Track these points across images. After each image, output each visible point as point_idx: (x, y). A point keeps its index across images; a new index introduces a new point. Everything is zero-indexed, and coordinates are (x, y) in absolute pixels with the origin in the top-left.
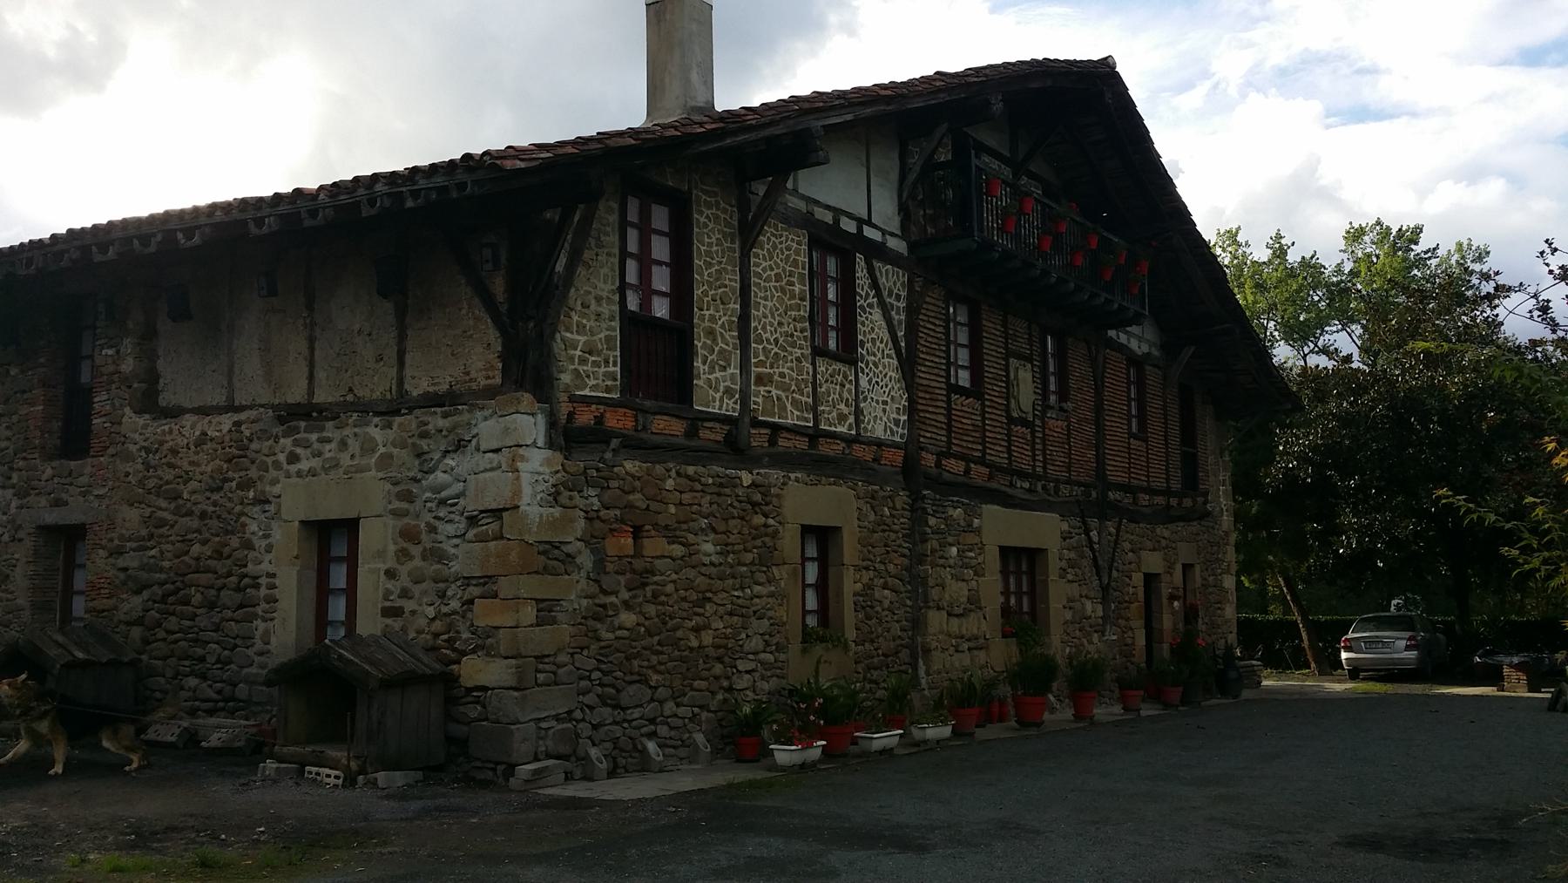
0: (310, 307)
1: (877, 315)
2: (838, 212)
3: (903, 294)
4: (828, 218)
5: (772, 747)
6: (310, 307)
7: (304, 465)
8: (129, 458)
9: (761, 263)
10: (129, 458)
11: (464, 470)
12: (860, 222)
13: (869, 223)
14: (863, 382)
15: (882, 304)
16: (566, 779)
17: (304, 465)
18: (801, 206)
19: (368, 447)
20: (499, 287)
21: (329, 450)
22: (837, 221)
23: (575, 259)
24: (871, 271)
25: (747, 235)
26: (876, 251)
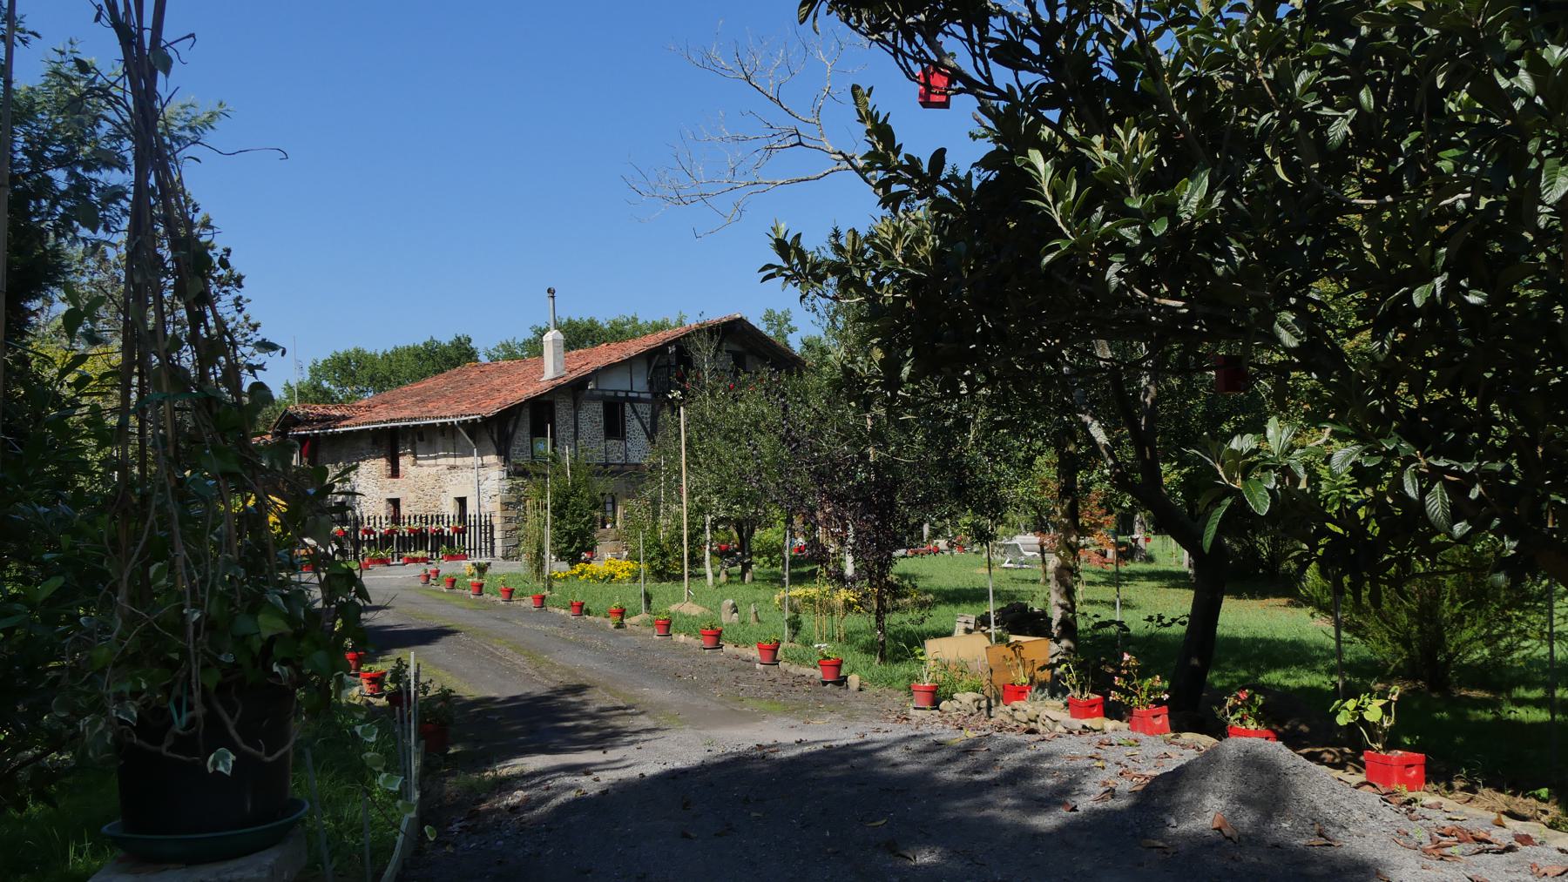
0: (454, 437)
1: (636, 422)
2: (616, 391)
3: (649, 412)
4: (612, 394)
5: (1426, 471)
6: (454, 437)
7: (454, 482)
8: (410, 479)
9: (583, 415)
10: (410, 479)
11: (1101, 66)
12: (627, 392)
13: (632, 391)
14: (629, 445)
15: (638, 417)
16: (453, 581)
17: (454, 482)
18: (600, 393)
19: (468, 478)
20: (495, 436)
21: (459, 478)
22: (616, 394)
23: (515, 426)
24: (633, 407)
25: (576, 407)
26: (638, 400)
